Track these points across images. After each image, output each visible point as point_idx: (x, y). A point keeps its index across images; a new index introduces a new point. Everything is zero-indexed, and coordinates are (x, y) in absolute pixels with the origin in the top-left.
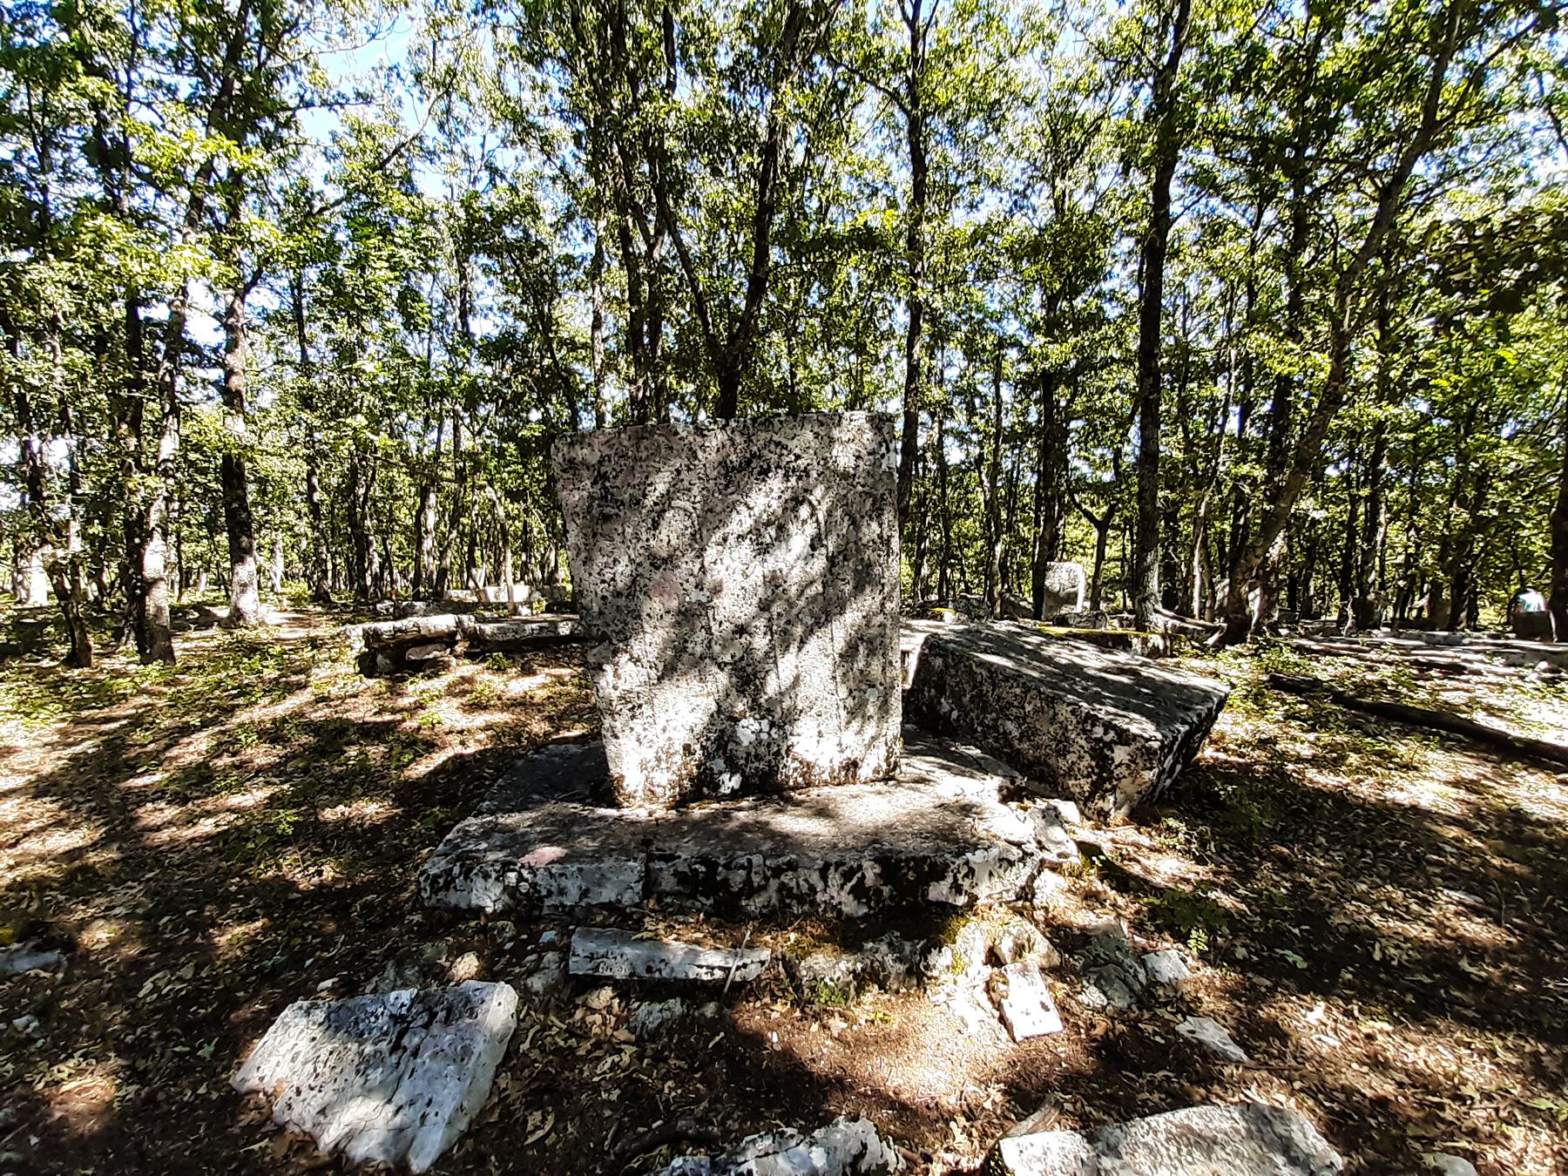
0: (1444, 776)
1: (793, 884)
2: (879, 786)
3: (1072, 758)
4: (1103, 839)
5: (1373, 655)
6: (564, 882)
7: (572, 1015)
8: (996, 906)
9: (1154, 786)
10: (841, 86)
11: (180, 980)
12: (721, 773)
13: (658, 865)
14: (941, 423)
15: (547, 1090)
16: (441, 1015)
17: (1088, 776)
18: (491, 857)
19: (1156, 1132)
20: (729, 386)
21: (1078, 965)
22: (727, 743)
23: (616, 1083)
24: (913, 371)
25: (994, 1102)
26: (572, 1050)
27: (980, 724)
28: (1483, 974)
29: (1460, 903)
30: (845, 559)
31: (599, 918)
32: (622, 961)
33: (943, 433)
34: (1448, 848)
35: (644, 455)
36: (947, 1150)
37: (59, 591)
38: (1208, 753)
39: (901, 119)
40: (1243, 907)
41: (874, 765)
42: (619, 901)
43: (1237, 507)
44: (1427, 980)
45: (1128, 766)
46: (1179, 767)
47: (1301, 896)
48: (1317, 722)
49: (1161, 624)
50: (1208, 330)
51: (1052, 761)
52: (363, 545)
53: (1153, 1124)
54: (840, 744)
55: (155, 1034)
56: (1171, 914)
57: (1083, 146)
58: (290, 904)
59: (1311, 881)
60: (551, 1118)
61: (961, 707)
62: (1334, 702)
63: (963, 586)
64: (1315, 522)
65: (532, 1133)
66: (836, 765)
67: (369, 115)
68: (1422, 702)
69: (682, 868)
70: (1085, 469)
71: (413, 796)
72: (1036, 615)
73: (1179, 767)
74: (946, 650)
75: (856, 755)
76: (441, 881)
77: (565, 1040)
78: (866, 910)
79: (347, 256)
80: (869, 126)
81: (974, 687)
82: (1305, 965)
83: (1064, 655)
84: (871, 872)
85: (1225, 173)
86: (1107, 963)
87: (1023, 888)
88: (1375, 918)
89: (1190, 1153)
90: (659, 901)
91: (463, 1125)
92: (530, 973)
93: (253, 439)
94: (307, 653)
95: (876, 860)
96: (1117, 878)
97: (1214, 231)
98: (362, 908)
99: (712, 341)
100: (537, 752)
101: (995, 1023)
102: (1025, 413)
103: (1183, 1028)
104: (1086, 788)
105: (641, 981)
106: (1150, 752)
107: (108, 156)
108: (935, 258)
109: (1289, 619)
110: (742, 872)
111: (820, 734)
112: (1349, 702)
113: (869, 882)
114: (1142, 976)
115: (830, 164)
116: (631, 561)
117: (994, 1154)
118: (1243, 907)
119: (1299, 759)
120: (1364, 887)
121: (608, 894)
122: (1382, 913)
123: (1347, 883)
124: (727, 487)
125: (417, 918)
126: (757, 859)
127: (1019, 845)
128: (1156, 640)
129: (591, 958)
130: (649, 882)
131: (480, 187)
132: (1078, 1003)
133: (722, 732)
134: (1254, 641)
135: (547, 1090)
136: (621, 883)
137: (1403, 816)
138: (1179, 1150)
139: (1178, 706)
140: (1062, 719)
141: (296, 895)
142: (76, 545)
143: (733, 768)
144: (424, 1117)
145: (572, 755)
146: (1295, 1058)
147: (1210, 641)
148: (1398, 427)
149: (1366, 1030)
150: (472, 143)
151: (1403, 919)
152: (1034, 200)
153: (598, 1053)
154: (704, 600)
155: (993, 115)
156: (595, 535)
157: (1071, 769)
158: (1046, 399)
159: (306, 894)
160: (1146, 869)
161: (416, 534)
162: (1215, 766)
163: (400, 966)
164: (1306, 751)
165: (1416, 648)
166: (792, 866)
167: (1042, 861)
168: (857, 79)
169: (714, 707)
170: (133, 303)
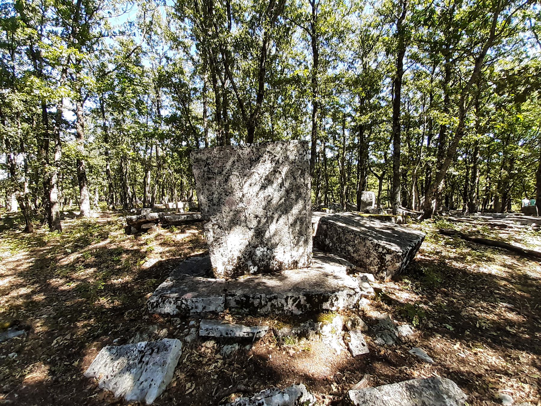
2: (305, 270)
3: (371, 259)
4: (382, 287)
6: (197, 304)
7: (200, 350)
9: (400, 268)
11: (66, 339)
12: (250, 266)
16: (156, 350)
17: (377, 265)
21: (375, 330)
22: (252, 256)
23: (216, 373)
26: (201, 362)
29: (506, 307)
30: (292, 191)
31: (209, 316)
33: (325, 147)
34: (502, 288)
38: (418, 256)
39: (309, 37)
40: (431, 310)
41: (303, 262)
42: (216, 311)
43: (427, 171)
45: (391, 262)
46: (408, 262)
48: (456, 245)
50: (416, 110)
51: (364, 260)
53: (401, 385)
54: (291, 255)
55: (57, 358)
56: (405, 312)
59: (455, 300)
60: (194, 385)
61: (333, 242)
64: (454, 176)
65: (187, 390)
66: (290, 262)
69: (238, 299)
70: (375, 159)
73: (408, 262)
75: (297, 259)
76: (155, 304)
77: (198, 358)
78: (301, 312)
79: (117, 89)
81: (337, 235)
82: (453, 329)
83: (369, 224)
84: (303, 299)
86: (384, 329)
87: (355, 304)
88: (477, 313)
91: (164, 388)
92: (186, 335)
95: (304, 295)
97: (418, 76)
100: (187, 259)
101: (346, 350)
102: (353, 140)
103: (411, 352)
104: (377, 269)
105: (224, 338)
106: (399, 257)
107: (34, 55)
113: (302, 303)
114: (397, 334)
115: (284, 55)
116: (219, 193)
118: (431, 310)
119: (450, 258)
120: (473, 302)
121: (212, 308)
122: (479, 311)
124: (251, 167)
125: (147, 317)
126: (263, 295)
127: (353, 289)
128: (400, 218)
129: (207, 330)
132: (375, 343)
134: (434, 218)
137: (486, 277)
138: (410, 393)
139: (408, 241)
140: (368, 245)
142: (27, 191)
143: (255, 264)
144: (150, 385)
147: (419, 218)
151: (486, 313)
152: (356, 65)
153: (210, 362)
155: (341, 36)
157: (371, 263)
158: (361, 135)
159: (108, 309)
162: (421, 261)
163: (141, 333)
164: (452, 255)
167: (361, 295)
169: (248, 243)
170: (44, 107)
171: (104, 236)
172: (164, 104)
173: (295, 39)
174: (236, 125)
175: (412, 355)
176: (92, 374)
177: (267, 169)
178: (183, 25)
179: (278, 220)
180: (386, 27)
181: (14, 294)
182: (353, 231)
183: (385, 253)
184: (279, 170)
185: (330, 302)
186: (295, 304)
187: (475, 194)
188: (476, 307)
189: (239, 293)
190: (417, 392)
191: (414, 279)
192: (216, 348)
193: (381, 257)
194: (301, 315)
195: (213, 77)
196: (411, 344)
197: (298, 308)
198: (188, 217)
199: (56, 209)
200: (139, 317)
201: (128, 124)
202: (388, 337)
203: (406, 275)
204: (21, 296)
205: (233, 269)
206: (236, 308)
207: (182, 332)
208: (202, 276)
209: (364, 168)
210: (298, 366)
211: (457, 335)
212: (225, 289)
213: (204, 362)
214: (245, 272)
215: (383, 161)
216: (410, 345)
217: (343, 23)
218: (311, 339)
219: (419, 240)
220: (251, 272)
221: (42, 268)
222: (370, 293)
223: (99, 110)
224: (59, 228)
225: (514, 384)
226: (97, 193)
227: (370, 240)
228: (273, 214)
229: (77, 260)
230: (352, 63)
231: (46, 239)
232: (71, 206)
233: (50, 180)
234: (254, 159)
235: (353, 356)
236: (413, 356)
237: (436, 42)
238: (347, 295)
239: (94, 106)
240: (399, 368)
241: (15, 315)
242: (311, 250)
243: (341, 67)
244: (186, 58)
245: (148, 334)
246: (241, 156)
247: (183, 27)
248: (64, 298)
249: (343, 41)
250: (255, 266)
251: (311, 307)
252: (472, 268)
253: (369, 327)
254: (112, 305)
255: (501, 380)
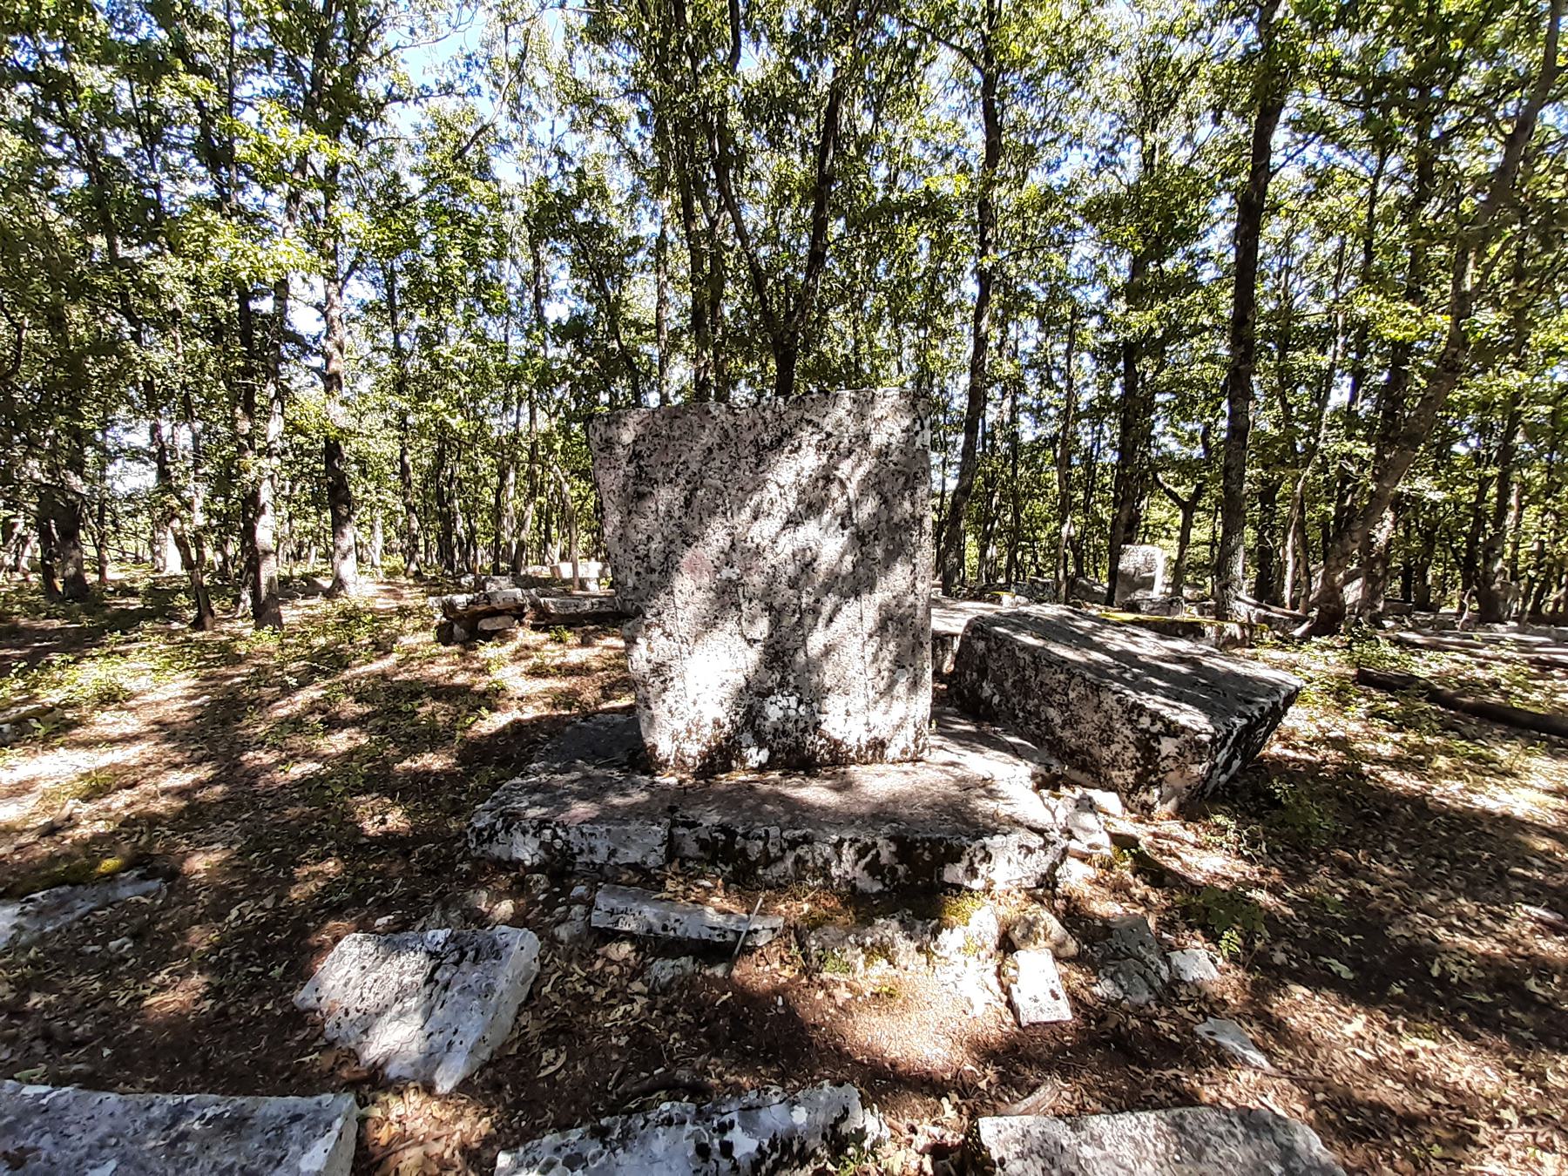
0: (1548, 785)
1: (809, 857)
2: (908, 767)
3: (1115, 748)
4: (1142, 833)
5: (1486, 652)
6: (593, 842)
7: (592, 965)
8: (1015, 892)
9: (1205, 781)
10: (911, 45)
11: (262, 909)
13: (680, 831)
14: (1014, 399)
15: (563, 1031)
16: (471, 954)
17: (1133, 767)
18: (531, 813)
19: (1144, 1128)
20: (785, 365)
21: (1097, 957)
22: (755, 718)
23: (626, 1030)
24: (981, 342)
25: (989, 1083)
26: (589, 996)
27: (1023, 709)
28: (1550, 994)
29: (1540, 920)
30: (876, 538)
31: (625, 877)
32: (642, 916)
33: (1014, 410)
34: (1537, 862)
35: (677, 434)
36: (935, 1124)
37: (187, 564)
38: (1275, 749)
39: (977, 77)
40: (1289, 911)
41: (902, 745)
43: (1343, 486)
44: (1486, 999)
45: (1176, 759)
46: (1236, 763)
47: (1359, 904)
48: (1403, 722)
49: (1243, 612)
50: (1317, 293)
51: (1095, 751)
52: (448, 520)
53: (1143, 1119)
54: (868, 724)
55: (235, 955)
56: (1204, 910)
57: (1178, 94)
58: (360, 847)
59: (1373, 890)
60: (563, 1057)
61: (1003, 693)
62: (1428, 701)
63: (1034, 569)
64: (1435, 505)
65: (545, 1067)
66: (863, 743)
67: (449, 105)
68: (1537, 704)
69: (705, 835)
70: (1174, 446)
71: (479, 753)
72: (1109, 601)
73: (1236, 763)
74: (989, 633)
75: (883, 734)
77: (584, 987)
78: (880, 887)
79: (427, 245)
80: (941, 86)
81: (1018, 671)
82: (1351, 976)
83: (1118, 642)
84: (886, 851)
85: (1340, 118)
86: (1128, 957)
87: (1043, 876)
88: (1441, 932)
89: (1178, 1152)
90: (682, 865)
91: (484, 1055)
92: (558, 923)
93: (351, 423)
94: (396, 622)
95: (891, 839)
96: (1152, 873)
97: (1322, 180)
98: (420, 854)
99: (768, 315)
100: (585, 720)
101: (1002, 1007)
102: (1108, 386)
103: (1201, 1029)
104: (1130, 780)
105: (657, 938)
106: (1199, 747)
107: (215, 155)
108: (1009, 223)
109: (1400, 610)
110: (761, 843)
111: (848, 713)
112: (1448, 702)
113: (884, 860)
114: (1164, 973)
115: (900, 130)
116: (665, 538)
117: (973, 1132)
118: (1289, 911)
119: (1378, 760)
120: (1433, 899)
121: (634, 856)
122: (1450, 928)
123: (1413, 893)
124: (757, 465)
125: (466, 867)
126: (774, 831)
127: (1041, 832)
128: (1233, 629)
129: (612, 913)
130: (672, 848)
131: (551, 172)
132: (1091, 994)
133: (750, 707)
134: (1348, 631)
135: (563, 1031)
136: (646, 845)
137: (1492, 826)
138: (1167, 1148)
139: (1239, 699)
140: (1106, 707)
141: (365, 840)
142: (200, 519)
143: (761, 743)
144: (450, 1044)
145: (615, 725)
146: (1323, 1069)
147: (1298, 632)
148: (1538, 399)
149: (1407, 1046)
150: (541, 131)
151: (1471, 935)
152: (1123, 155)
153: (612, 1001)
154: (735, 577)
155: (1072, 65)
156: (630, 513)
157: (1114, 760)
158: (1131, 377)
159: (374, 839)
160: (1185, 865)
161: (497, 512)
162: (1278, 763)
163: (445, 908)
164: (1386, 750)
165: (1540, 645)
166: (807, 840)
167: (1065, 851)
168: (929, 38)
169: (743, 683)
170: (245, 297)
171: (382, 648)
172: (556, 287)
173: (934, 81)
174: (740, 342)
175: (1203, 1041)
176: (312, 1002)
177: (806, 473)
178: (608, 58)
179: (831, 620)
180: (1224, 32)
181: (148, 786)
182: (1065, 661)
183: (1160, 733)
184: (838, 473)
185: (965, 863)
186: (863, 863)
187: (1499, 564)
188: (1439, 917)
189: (713, 818)
190: (1188, 1145)
191: (1244, 815)
192: (632, 962)
193: (1147, 746)
194: (879, 894)
195: (687, 203)
196: (1212, 1006)
197: (872, 874)
198: (601, 603)
199: (270, 570)
200: (448, 864)
201: (454, 344)
202: (1137, 979)
203: (1224, 803)
204: (165, 792)
205: (700, 753)
206: (699, 860)
207: (550, 914)
208: (617, 767)
209: (1135, 479)
210: (854, 1036)
211: (1363, 991)
212: (672, 806)
213: (597, 999)
214: (734, 763)
215: (1198, 451)
216: (1200, 1011)
217: (1085, 27)
218: (903, 964)
219: (1276, 698)
220: (752, 763)
221: (224, 723)
222: (1097, 847)
223: (384, 306)
224: (277, 620)
225: (1513, 1151)
226: (378, 530)
227: (1115, 693)
228: (817, 601)
229: (313, 707)
230: (1111, 150)
231: (242, 648)
232: (312, 564)
233: (255, 496)
234: (767, 442)
235: (1019, 1025)
236: (1204, 1043)
237: (1386, 78)
238: (1021, 847)
239: (370, 294)
240: (1157, 1073)
241: (144, 839)
242: (927, 713)
243: (1076, 163)
244: (613, 152)
245: (463, 911)
246: (732, 433)
247: (609, 64)
248: (269, 803)
249: (1079, 84)
250: (760, 748)
251: (916, 873)
252: (1449, 791)
253: (1079, 946)
254: (383, 828)
255: (1474, 1137)
